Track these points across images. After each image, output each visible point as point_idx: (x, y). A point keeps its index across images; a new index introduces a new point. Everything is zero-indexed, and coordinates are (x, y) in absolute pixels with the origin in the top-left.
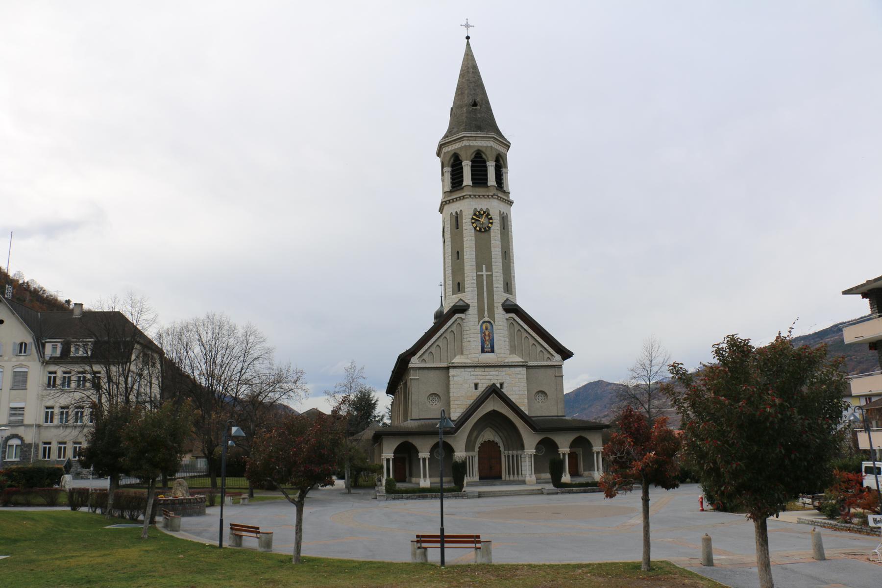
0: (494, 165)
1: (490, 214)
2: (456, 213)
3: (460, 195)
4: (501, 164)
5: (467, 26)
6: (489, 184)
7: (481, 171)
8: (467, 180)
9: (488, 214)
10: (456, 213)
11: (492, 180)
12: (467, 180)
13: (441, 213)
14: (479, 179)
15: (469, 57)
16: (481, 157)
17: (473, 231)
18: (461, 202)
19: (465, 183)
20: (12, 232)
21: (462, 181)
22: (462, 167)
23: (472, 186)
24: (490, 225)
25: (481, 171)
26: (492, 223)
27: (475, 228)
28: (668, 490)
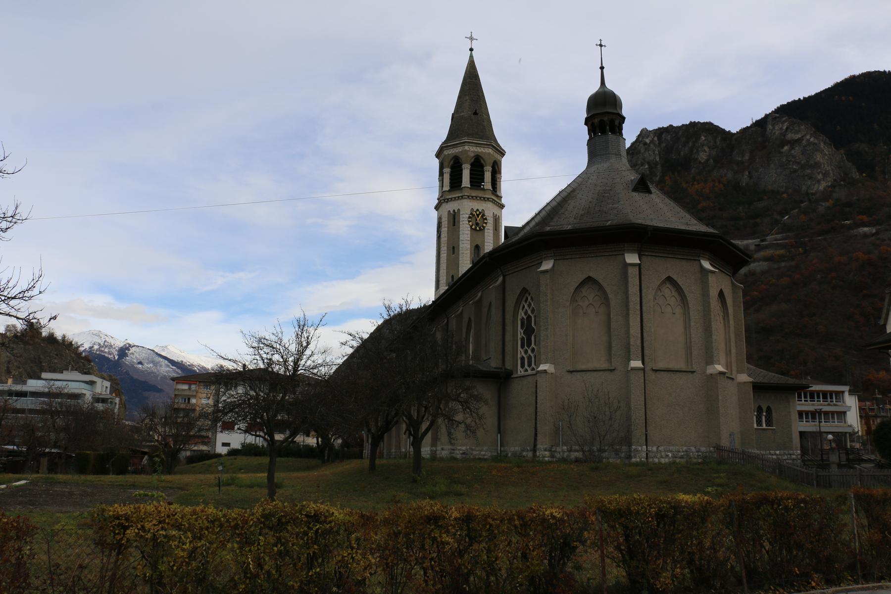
1: (486, 214)
2: (454, 211)
5: (471, 39)
8: (466, 181)
9: (484, 215)
10: (454, 211)
11: (487, 184)
12: (466, 181)
16: (459, 162)
17: (469, 229)
18: (459, 201)
23: (449, 191)
24: (484, 225)
26: (486, 223)
27: (471, 227)
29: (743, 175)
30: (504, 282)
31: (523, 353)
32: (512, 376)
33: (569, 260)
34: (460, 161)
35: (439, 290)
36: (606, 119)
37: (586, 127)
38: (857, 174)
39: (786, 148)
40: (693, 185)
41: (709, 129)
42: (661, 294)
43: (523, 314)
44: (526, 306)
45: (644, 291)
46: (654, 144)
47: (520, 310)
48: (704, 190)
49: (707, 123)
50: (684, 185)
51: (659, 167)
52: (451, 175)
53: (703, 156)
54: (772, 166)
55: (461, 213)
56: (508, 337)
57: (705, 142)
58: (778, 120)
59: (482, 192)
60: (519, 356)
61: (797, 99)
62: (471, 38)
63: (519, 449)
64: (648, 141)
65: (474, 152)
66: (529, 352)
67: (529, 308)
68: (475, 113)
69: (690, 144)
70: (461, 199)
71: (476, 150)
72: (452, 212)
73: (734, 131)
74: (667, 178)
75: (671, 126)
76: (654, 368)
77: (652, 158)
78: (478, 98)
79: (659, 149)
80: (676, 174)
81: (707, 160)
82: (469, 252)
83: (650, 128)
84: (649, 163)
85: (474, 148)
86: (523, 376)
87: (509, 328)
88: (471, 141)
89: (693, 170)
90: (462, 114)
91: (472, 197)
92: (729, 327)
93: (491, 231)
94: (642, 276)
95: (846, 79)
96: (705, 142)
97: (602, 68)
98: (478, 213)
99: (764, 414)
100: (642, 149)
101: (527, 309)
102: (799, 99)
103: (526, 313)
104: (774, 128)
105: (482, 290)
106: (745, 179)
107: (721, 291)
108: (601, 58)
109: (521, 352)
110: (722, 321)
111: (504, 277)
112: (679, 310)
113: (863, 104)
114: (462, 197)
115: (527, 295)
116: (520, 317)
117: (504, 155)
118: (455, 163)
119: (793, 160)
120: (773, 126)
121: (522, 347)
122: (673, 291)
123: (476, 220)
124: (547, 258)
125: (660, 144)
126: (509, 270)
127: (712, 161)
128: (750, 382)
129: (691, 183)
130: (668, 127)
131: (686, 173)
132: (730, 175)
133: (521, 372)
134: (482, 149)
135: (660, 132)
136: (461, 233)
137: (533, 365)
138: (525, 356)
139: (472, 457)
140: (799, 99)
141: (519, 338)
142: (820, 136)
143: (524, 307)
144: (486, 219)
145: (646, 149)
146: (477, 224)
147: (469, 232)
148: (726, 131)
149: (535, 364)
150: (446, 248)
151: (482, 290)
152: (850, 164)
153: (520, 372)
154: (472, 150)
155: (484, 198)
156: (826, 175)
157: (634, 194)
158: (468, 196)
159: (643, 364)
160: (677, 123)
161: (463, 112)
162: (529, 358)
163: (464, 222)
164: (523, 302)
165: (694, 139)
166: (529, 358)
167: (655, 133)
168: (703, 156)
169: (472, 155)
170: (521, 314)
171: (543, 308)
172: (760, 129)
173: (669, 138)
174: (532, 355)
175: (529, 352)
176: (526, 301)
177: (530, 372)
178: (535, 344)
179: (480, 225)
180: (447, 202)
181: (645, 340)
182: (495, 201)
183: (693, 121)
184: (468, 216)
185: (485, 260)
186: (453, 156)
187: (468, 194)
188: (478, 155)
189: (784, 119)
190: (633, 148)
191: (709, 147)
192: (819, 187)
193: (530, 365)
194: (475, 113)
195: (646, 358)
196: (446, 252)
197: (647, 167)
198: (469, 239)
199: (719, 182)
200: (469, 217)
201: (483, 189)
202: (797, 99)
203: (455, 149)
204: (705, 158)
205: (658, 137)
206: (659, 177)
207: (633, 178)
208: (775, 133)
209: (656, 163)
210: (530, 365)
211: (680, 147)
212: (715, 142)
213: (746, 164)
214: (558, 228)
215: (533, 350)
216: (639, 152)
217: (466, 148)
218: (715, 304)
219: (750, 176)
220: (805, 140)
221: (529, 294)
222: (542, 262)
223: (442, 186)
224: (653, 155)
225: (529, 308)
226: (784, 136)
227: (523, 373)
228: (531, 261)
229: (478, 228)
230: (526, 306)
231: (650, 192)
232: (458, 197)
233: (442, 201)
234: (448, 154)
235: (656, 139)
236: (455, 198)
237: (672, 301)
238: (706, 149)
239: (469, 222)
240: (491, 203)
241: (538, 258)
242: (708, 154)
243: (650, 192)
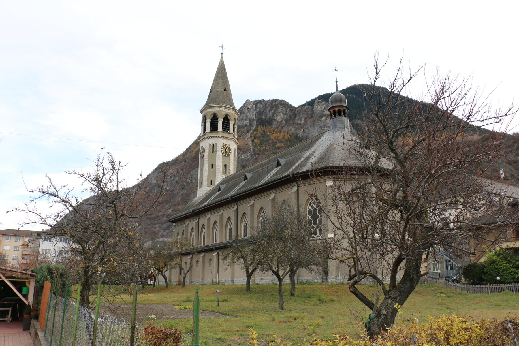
0: (210, 121)
2: (213, 144)
3: (217, 135)
5: (222, 48)
8: (220, 127)
9: (229, 148)
12: (220, 127)
16: (216, 117)
17: (222, 155)
18: (216, 139)
19: (219, 130)
22: (218, 121)
23: (210, 132)
24: (230, 153)
26: (231, 153)
27: (223, 154)
29: (300, 131)
30: (298, 190)
36: (341, 109)
39: (323, 118)
40: (273, 134)
41: (284, 104)
46: (253, 109)
47: (308, 205)
48: (279, 137)
49: (283, 100)
50: (269, 134)
51: (255, 122)
52: (211, 124)
53: (279, 119)
54: (316, 127)
55: (217, 146)
57: (281, 111)
58: (320, 103)
59: (228, 134)
61: (328, 93)
63: (311, 278)
64: (249, 107)
65: (225, 112)
68: (225, 90)
69: (273, 111)
71: (226, 111)
72: (211, 144)
73: (296, 106)
74: (259, 128)
75: (263, 100)
77: (251, 117)
80: (264, 127)
81: (282, 121)
83: (251, 100)
84: (249, 119)
85: (225, 110)
89: (274, 126)
90: (218, 89)
91: (224, 137)
93: (233, 157)
95: (352, 86)
96: (281, 111)
97: (337, 82)
98: (226, 146)
100: (246, 111)
102: (329, 93)
103: (312, 207)
104: (318, 107)
106: (301, 133)
108: (423, 91)
113: (360, 100)
114: (218, 136)
115: (263, 210)
118: (213, 117)
119: (327, 125)
120: (317, 106)
123: (226, 150)
125: (256, 109)
127: (284, 122)
129: (272, 133)
130: (261, 100)
131: (270, 127)
132: (293, 130)
134: (229, 110)
135: (257, 103)
136: (217, 157)
139: (285, 283)
140: (329, 93)
144: (230, 150)
145: (248, 111)
146: (226, 153)
148: (511, 135)
150: (207, 165)
152: (354, 130)
154: (224, 110)
155: (230, 138)
158: (222, 137)
160: (266, 99)
161: (218, 88)
165: (275, 109)
167: (254, 103)
168: (279, 119)
169: (224, 113)
170: (244, 224)
172: (310, 107)
173: (261, 106)
179: (227, 153)
180: (209, 138)
183: (275, 99)
184: (221, 148)
186: (213, 113)
187: (222, 136)
188: (227, 114)
189: (323, 103)
190: (241, 110)
191: (283, 114)
196: (207, 167)
197: (248, 121)
198: (222, 161)
199: (288, 134)
200: (222, 149)
201: (229, 133)
203: (214, 109)
204: (281, 119)
205: (255, 105)
206: (254, 127)
208: (318, 110)
209: (253, 120)
211: (267, 112)
212: (286, 111)
213: (302, 125)
216: (245, 113)
217: (221, 109)
219: (304, 132)
224: (252, 115)
226: (323, 112)
229: (226, 155)
232: (216, 136)
234: (210, 112)
235: (254, 106)
238: (281, 114)
239: (222, 151)
240: (233, 141)
242: (282, 117)
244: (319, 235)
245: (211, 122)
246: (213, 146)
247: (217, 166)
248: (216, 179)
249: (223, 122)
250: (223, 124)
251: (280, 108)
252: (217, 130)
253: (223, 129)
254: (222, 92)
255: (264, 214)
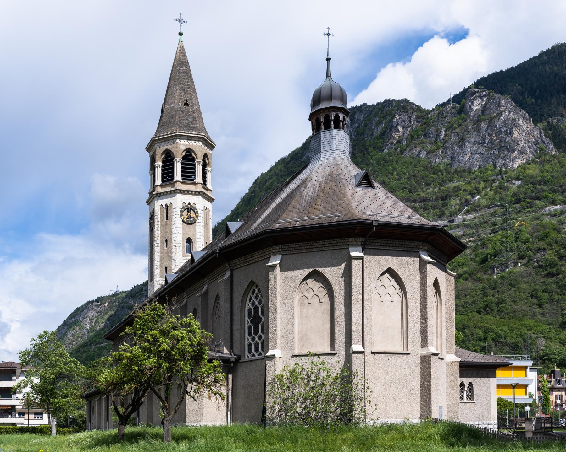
1: (197, 208)
2: (166, 205)
4: (193, 157)
5: (181, 21)
6: (196, 181)
7: (191, 169)
8: (178, 176)
10: (166, 205)
11: (199, 178)
12: (178, 176)
13: (149, 204)
14: (188, 175)
15: (181, 52)
16: (170, 156)
17: (182, 222)
20: (166, 241)
21: (173, 176)
25: (191, 169)
28: (410, 61)
30: (232, 276)
31: (250, 340)
32: (240, 361)
33: (296, 254)
34: (172, 155)
35: (153, 281)
37: (310, 123)
38: (554, 150)
42: (382, 284)
43: (250, 305)
44: (253, 298)
45: (365, 282)
47: (248, 302)
52: (162, 170)
56: (236, 326)
57: (400, 121)
60: (246, 342)
62: (181, 21)
66: (257, 339)
67: (257, 299)
68: (186, 104)
70: (173, 193)
72: (164, 206)
76: (372, 352)
78: (188, 88)
79: (351, 129)
82: (181, 245)
86: (251, 361)
87: (237, 318)
88: (183, 134)
92: (441, 312)
94: (365, 269)
99: (466, 389)
101: (255, 300)
103: (253, 304)
105: (208, 283)
107: (436, 280)
109: (248, 339)
110: (435, 307)
111: (232, 271)
112: (397, 299)
114: (174, 191)
115: (254, 287)
116: (247, 308)
117: (214, 147)
118: (166, 157)
121: (250, 334)
122: (393, 280)
124: (275, 253)
126: (236, 265)
128: (458, 362)
133: (248, 357)
137: (260, 351)
138: (252, 343)
141: (246, 327)
142: (520, 111)
143: (251, 298)
147: (181, 226)
149: (262, 350)
151: (208, 283)
153: (248, 356)
156: (522, 152)
157: (359, 189)
159: (363, 347)
162: (257, 344)
163: (176, 216)
164: (250, 294)
166: (257, 344)
170: (249, 305)
171: (271, 299)
174: (259, 342)
175: (257, 339)
176: (253, 293)
177: (257, 357)
178: (262, 332)
181: (365, 326)
182: (206, 194)
183: (388, 99)
184: (180, 210)
185: (214, 255)
192: (513, 165)
193: (257, 350)
194: (186, 104)
195: (366, 343)
196: (159, 245)
202: (499, 71)
207: (356, 173)
210: (257, 350)
214: (287, 225)
215: (260, 338)
218: (431, 290)
220: (503, 115)
221: (257, 286)
222: (270, 257)
223: (154, 180)
225: (257, 299)
227: (250, 357)
228: (259, 256)
230: (253, 298)
231: (372, 187)
233: (154, 196)
236: (167, 192)
237: (391, 291)
241: (266, 253)
243: (372, 187)
244: (255, 353)
245: (163, 166)
246: (167, 210)
247: (173, 242)
248: (173, 264)
249: (182, 164)
250: (182, 168)
251: (397, 117)
252: (173, 179)
253: (182, 176)
254: (180, 108)
255: (255, 295)
